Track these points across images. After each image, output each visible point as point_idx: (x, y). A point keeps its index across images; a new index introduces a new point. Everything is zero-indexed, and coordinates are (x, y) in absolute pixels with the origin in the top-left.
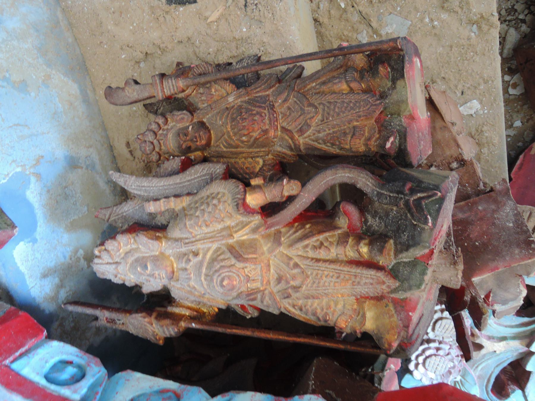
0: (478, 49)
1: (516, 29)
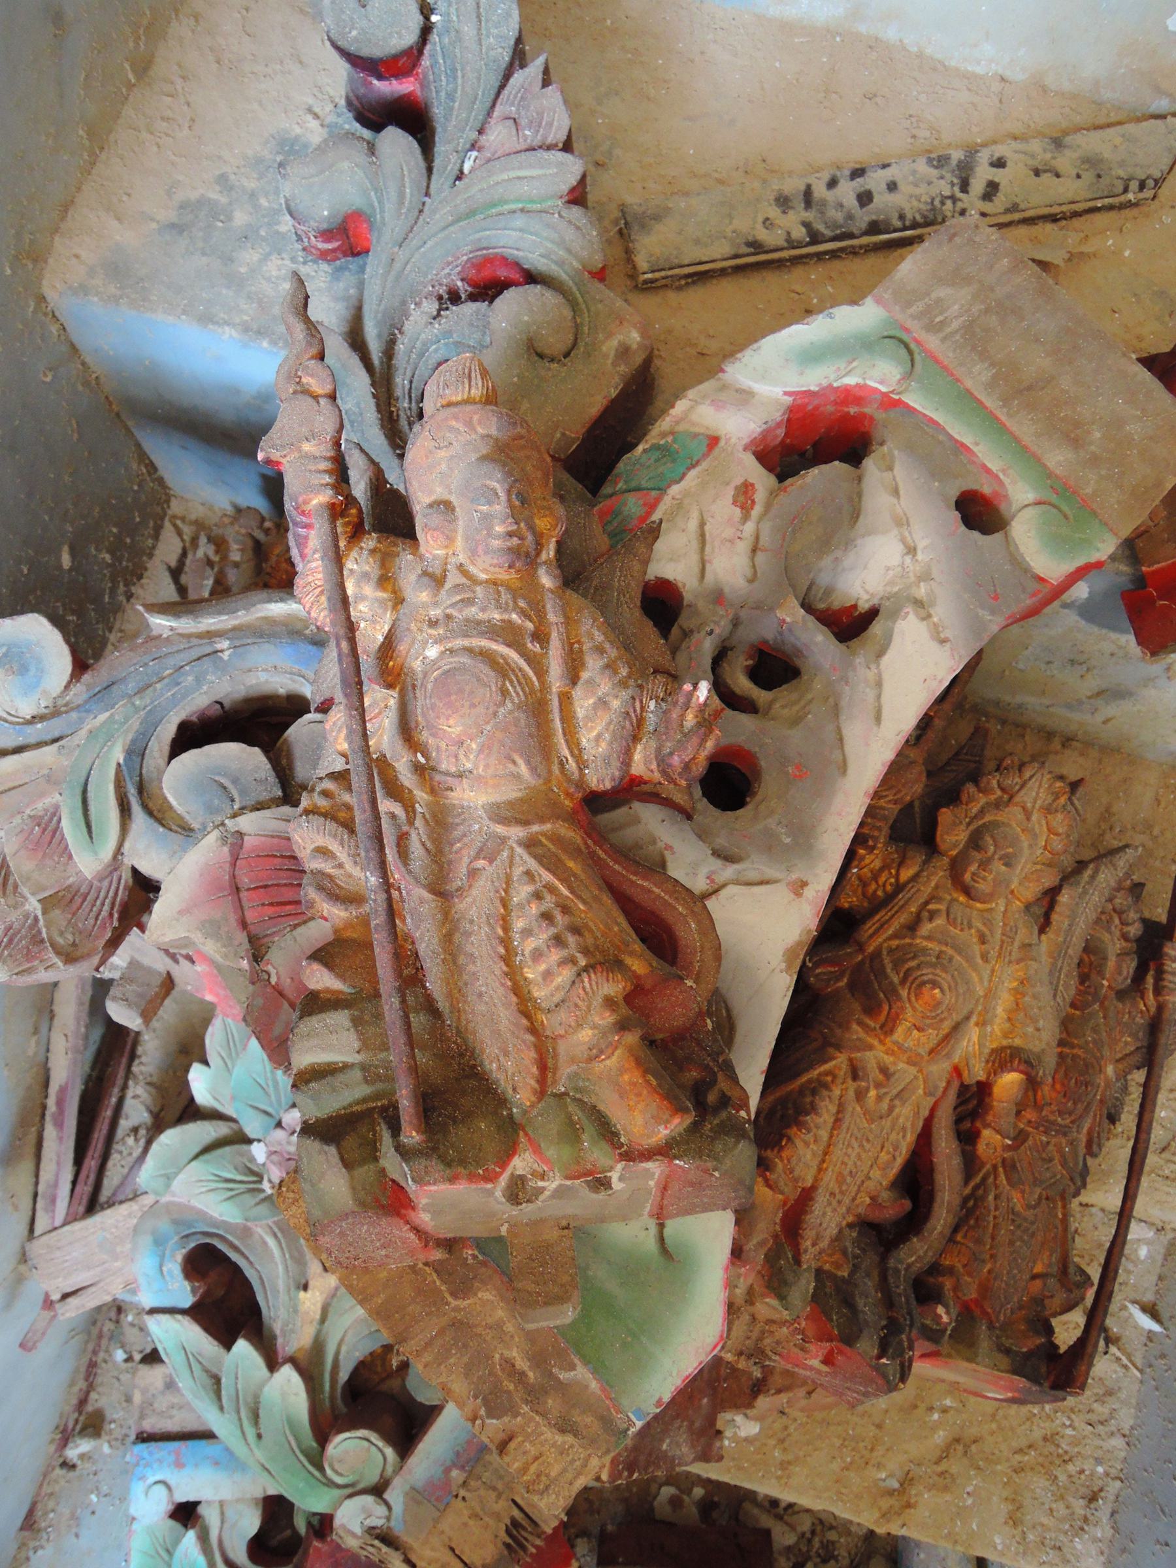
1: (789, 1549)
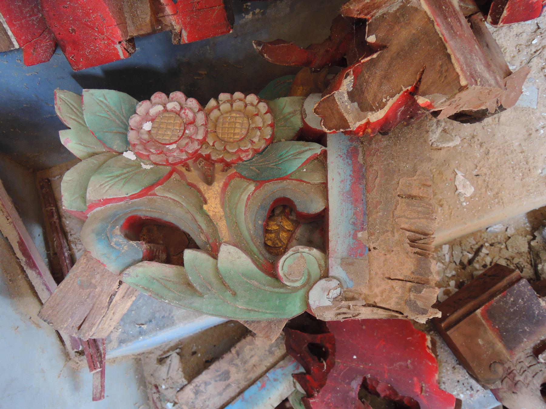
0: (527, 179)
